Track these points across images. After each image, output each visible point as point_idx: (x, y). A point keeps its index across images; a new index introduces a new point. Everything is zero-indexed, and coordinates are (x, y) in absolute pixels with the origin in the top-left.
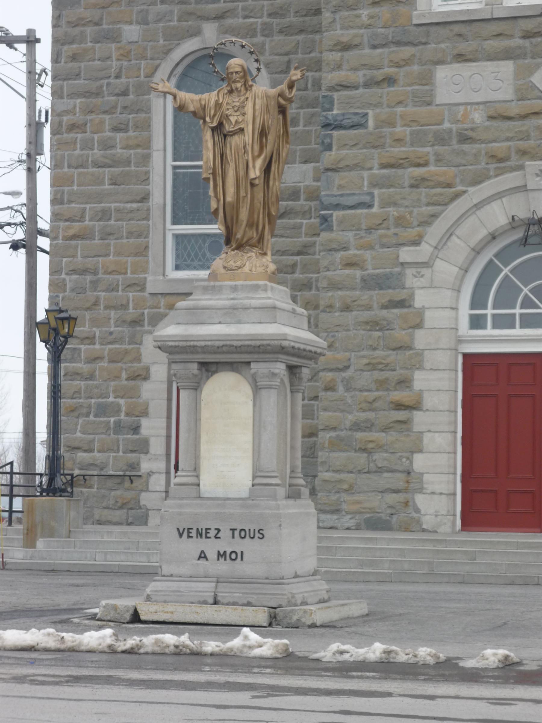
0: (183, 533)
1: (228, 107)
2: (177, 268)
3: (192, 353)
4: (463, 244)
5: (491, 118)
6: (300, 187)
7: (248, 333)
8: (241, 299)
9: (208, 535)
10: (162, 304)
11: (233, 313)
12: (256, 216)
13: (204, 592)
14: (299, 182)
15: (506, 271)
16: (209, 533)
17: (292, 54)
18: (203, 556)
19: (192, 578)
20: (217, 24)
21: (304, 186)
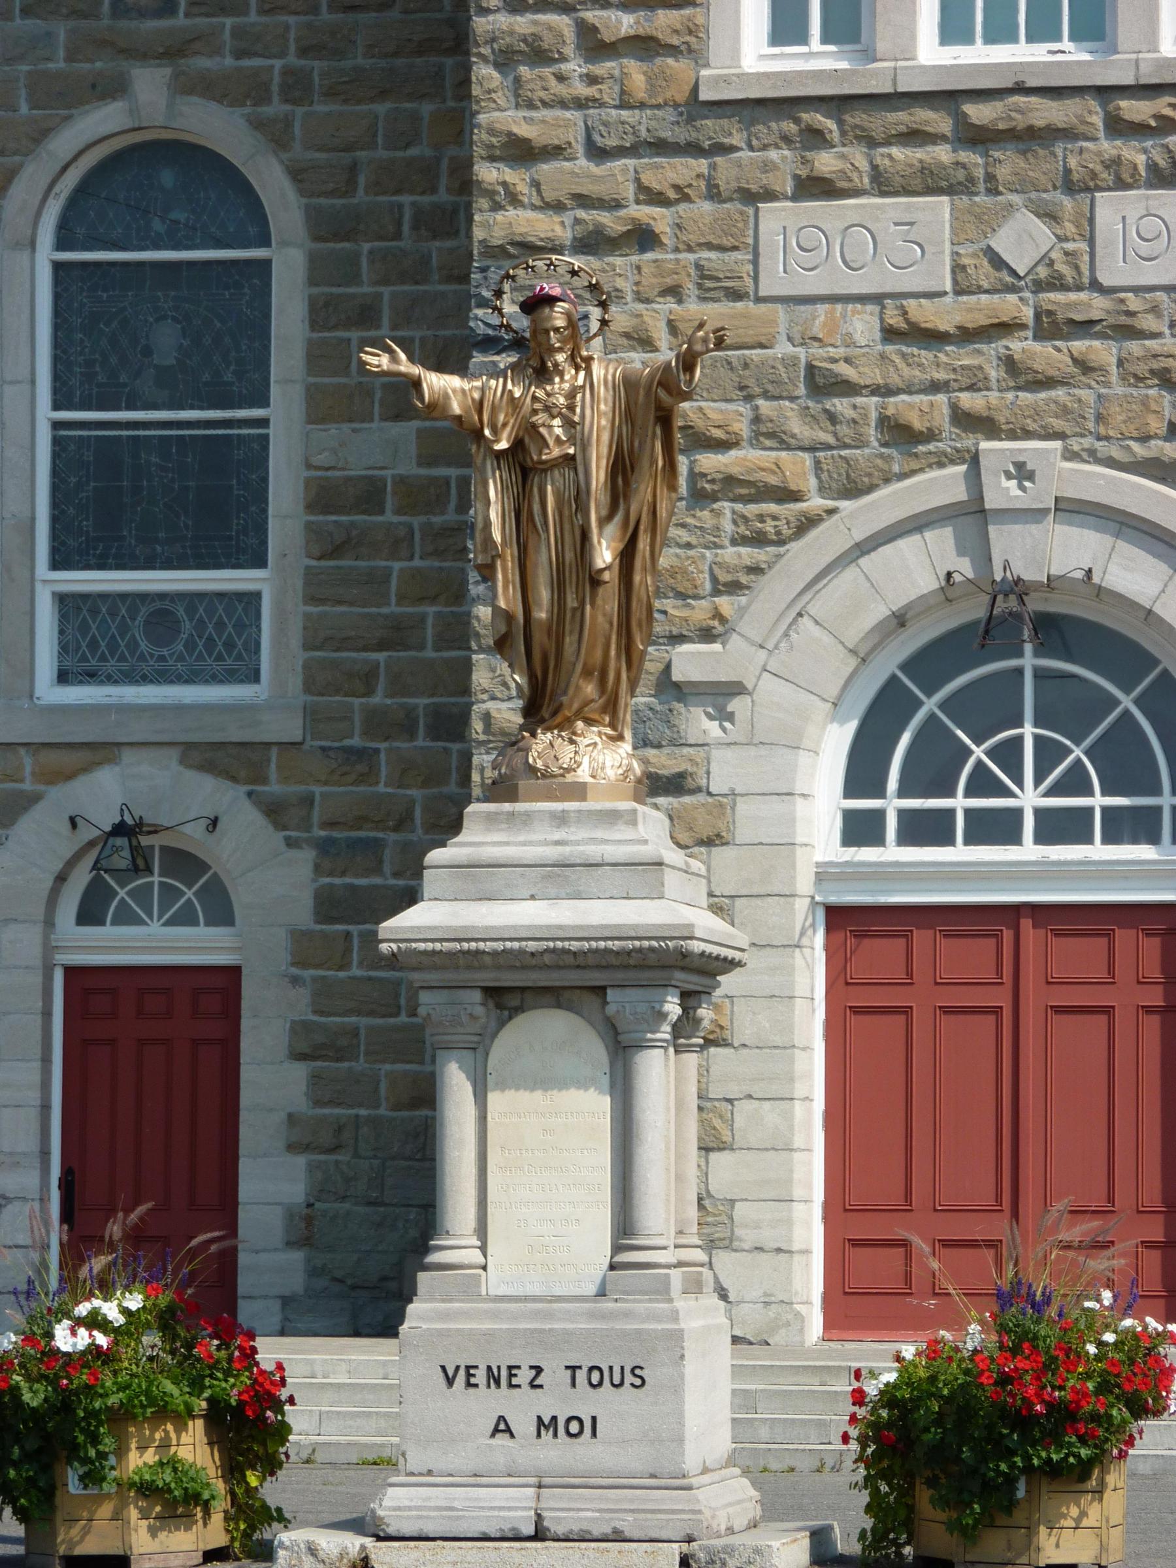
0: (455, 1376)
1: (537, 406)
2: (63, 677)
3: (469, 968)
4: (827, 639)
5: (890, 334)
6: (383, 480)
7: (604, 922)
8: (577, 843)
9: (514, 1381)
10: (28, 770)
11: (561, 876)
12: (598, 654)
13: (510, 1509)
14: (382, 468)
15: (930, 705)
16: (515, 1375)
17: (362, 149)
18: (502, 1427)
19: (477, 1477)
20: (168, 71)
21: (393, 476)
